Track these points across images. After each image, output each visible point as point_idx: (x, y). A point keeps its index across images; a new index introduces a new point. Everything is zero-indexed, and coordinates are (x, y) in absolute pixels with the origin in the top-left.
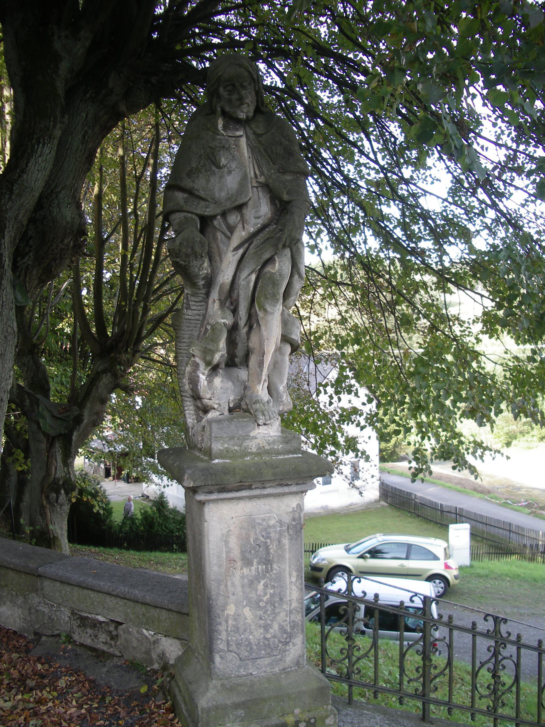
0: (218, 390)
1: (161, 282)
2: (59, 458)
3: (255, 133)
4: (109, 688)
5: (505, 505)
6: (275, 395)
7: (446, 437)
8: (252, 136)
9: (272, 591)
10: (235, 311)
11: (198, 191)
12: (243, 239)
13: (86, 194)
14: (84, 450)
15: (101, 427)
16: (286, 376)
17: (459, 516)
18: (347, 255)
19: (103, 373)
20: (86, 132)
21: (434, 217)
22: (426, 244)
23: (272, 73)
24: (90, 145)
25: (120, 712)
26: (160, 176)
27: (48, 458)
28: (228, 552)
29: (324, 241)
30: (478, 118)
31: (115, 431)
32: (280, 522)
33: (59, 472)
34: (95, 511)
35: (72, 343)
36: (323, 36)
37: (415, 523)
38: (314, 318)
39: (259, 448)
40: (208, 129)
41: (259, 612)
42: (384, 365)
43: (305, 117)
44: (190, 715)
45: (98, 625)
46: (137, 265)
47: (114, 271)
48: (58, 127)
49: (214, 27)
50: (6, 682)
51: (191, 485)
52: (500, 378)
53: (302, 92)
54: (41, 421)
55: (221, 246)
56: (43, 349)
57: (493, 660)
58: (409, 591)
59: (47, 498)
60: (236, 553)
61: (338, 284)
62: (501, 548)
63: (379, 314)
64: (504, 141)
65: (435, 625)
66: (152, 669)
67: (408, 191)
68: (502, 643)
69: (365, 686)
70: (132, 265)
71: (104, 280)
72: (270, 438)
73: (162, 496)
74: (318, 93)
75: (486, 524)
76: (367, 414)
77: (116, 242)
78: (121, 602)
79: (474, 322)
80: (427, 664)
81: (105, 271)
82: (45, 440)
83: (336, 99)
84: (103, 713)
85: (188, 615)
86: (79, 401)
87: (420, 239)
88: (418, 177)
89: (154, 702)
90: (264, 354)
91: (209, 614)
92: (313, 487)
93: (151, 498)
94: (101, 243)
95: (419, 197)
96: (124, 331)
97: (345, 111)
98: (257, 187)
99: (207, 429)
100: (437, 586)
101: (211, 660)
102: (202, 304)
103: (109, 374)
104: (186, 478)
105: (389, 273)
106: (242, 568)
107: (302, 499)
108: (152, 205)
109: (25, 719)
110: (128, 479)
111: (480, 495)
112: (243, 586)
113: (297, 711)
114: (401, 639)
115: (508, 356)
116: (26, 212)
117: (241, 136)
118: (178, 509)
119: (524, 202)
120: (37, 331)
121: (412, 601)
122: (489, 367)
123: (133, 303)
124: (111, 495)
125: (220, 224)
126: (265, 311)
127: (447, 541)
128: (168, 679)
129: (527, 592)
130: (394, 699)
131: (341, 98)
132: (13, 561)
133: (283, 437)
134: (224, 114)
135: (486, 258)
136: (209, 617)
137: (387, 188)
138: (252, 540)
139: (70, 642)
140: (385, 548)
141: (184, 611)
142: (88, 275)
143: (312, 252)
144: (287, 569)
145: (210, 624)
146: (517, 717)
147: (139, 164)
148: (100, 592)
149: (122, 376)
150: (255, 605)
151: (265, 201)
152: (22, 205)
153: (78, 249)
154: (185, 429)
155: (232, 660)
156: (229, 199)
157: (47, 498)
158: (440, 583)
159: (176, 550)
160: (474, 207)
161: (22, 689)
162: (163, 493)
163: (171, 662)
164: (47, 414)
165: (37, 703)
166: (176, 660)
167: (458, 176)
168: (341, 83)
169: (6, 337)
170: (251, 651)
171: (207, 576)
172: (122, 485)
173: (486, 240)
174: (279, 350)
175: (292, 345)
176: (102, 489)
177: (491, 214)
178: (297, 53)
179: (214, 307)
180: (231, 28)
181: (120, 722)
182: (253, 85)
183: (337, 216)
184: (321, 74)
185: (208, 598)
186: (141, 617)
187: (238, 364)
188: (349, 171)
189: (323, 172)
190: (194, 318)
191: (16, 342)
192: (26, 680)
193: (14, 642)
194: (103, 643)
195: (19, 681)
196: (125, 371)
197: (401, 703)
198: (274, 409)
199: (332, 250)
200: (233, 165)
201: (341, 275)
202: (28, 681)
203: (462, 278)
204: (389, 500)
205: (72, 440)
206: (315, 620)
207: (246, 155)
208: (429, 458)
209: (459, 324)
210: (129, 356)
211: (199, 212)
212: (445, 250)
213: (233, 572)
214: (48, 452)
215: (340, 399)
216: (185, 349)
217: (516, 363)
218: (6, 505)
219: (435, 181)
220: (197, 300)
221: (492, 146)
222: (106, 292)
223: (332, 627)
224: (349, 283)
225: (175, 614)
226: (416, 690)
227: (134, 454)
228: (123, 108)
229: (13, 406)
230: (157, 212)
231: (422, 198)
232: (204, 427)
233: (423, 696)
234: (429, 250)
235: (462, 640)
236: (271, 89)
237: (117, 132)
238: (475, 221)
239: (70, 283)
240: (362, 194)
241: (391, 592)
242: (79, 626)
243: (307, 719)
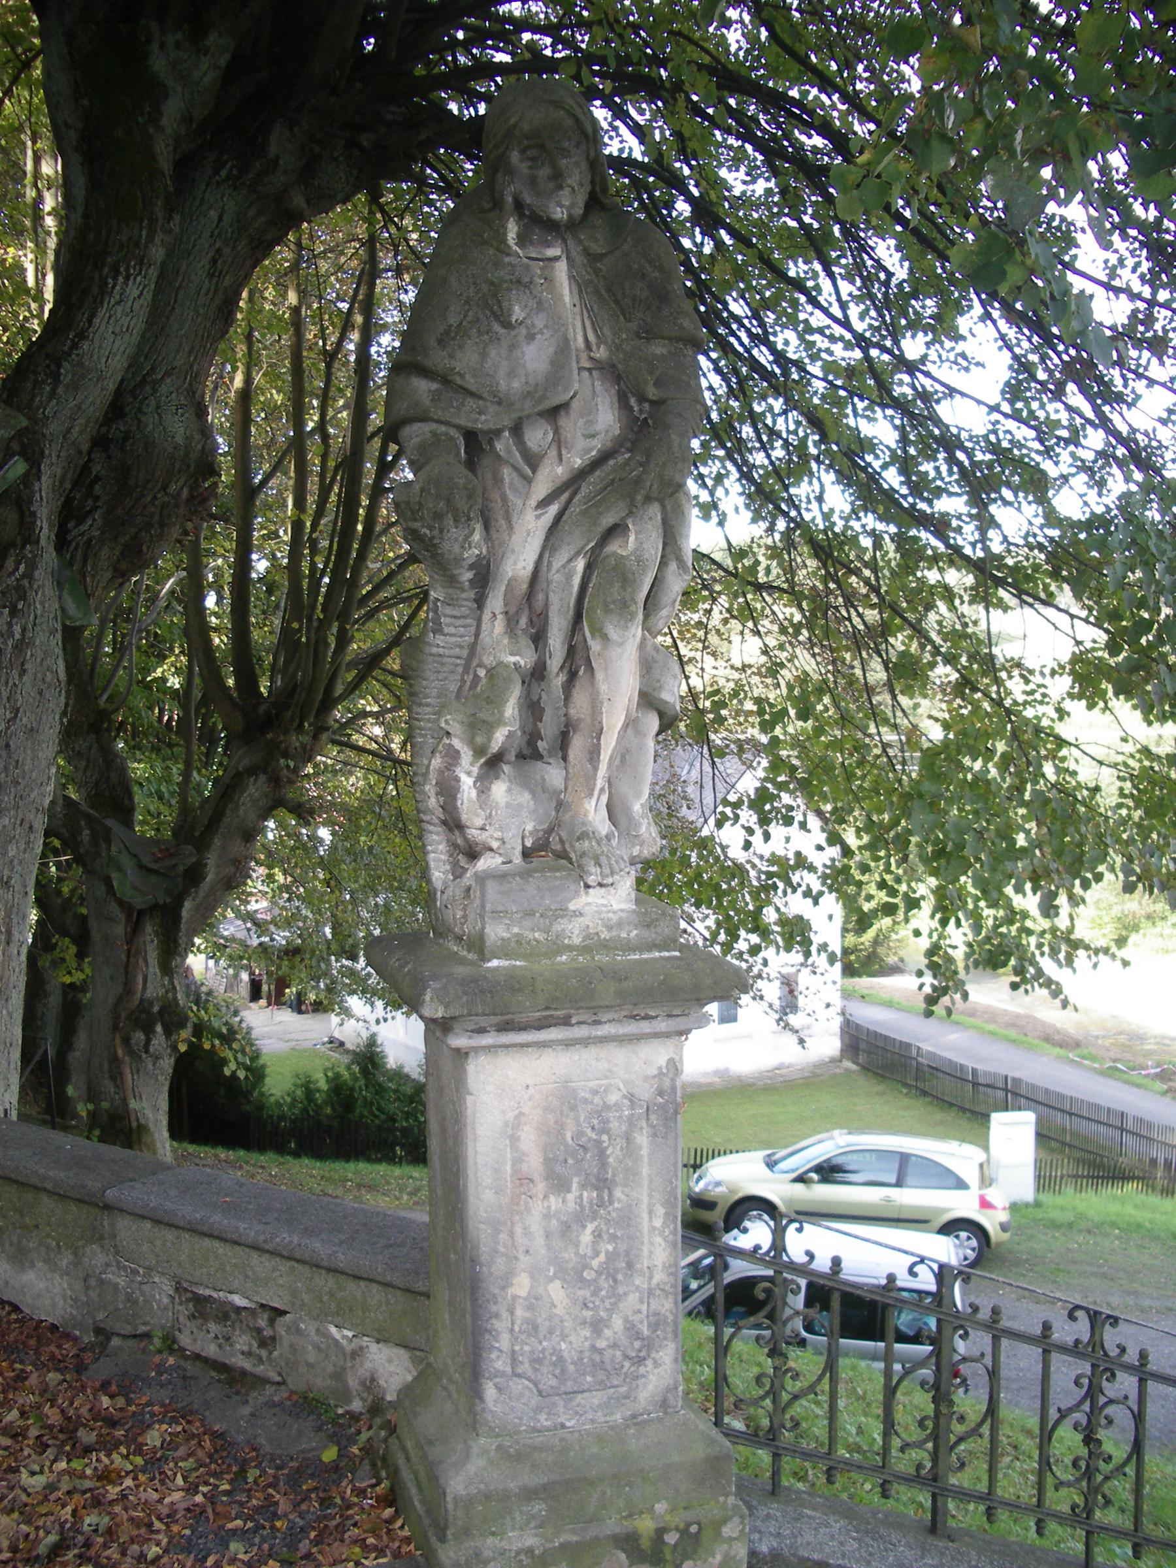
0: (500, 812)
1: (376, 580)
2: (153, 955)
3: (586, 252)
4: (254, 1449)
5: (1111, 1073)
6: (623, 822)
7: (996, 918)
8: (579, 259)
9: (610, 1248)
10: (539, 638)
11: (462, 376)
12: (558, 483)
13: (216, 388)
14: (207, 941)
15: (243, 892)
16: (649, 778)
17: (1013, 1095)
18: (781, 525)
19: (250, 775)
20: (218, 251)
21: (969, 445)
22: (953, 504)
23: (623, 130)
24: (228, 280)
25: (277, 1503)
26: (377, 352)
27: (128, 956)
28: (517, 1161)
29: (732, 496)
30: (1069, 231)
31: (274, 903)
32: (631, 1098)
33: (151, 984)
34: (227, 1072)
35: (185, 707)
36: (733, 49)
37: (917, 1108)
38: (709, 661)
39: (588, 937)
40: (485, 243)
41: (581, 1293)
42: (861, 763)
43: (693, 226)
44: (428, 1512)
45: (233, 1316)
46: (326, 544)
47: (274, 556)
48: (157, 240)
49: (498, 27)
50: (34, 1432)
51: (440, 1015)
52: (1108, 799)
53: (686, 171)
54: (115, 877)
55: (511, 496)
56: (122, 723)
57: (1086, 1407)
58: (906, 1252)
59: (126, 1041)
60: (534, 1164)
61: (759, 588)
62: (1101, 1166)
63: (848, 656)
64: (1125, 280)
65: (961, 1327)
66: (347, 1412)
67: (914, 388)
68: (1106, 1369)
69: (806, 1455)
70: (314, 544)
71: (254, 575)
72: (611, 915)
73: (372, 1042)
74: (723, 173)
75: (1071, 1114)
76: (825, 866)
77: (280, 493)
78: (284, 1266)
79: (1053, 673)
80: (944, 1410)
81: (254, 557)
82: (122, 917)
83: (760, 187)
84: (242, 1504)
85: (427, 1295)
86: (197, 834)
87: (938, 492)
88: (940, 357)
89: (351, 1481)
90: (601, 732)
91: (472, 1294)
92: (704, 1020)
93: (349, 1046)
94: (248, 493)
95: (938, 401)
96: (296, 686)
97: (780, 214)
98: (589, 370)
99: (476, 893)
100: (961, 1246)
101: (476, 1393)
102: (469, 621)
103: (262, 778)
104: (427, 998)
105: (873, 566)
106: (545, 1197)
107: (679, 1048)
108: (360, 414)
109: (74, 1512)
110: (298, 1006)
111: (1058, 1051)
112: (548, 1236)
113: (661, 1507)
114: (888, 1357)
115: (1129, 748)
116: (88, 422)
117: (556, 259)
118: (406, 1070)
119: (1165, 415)
120: (109, 682)
121: (912, 1272)
122: (1086, 773)
123: (315, 624)
124: (264, 1038)
125: (509, 452)
126: (605, 638)
127: (986, 1148)
128: (383, 1433)
129: (1157, 1262)
130: (868, 1486)
131: (772, 184)
132: (51, 1174)
133: (638, 914)
135: (1083, 536)
136: (474, 1300)
137: (873, 382)
138: (568, 1135)
139: (171, 1351)
140: (850, 1162)
141: (420, 1286)
142: (219, 564)
143: (706, 517)
144: (645, 1200)
145: (476, 1317)
146: (1136, 1530)
147: (332, 324)
148: (239, 1244)
149: (291, 782)
150: (574, 1276)
151: (608, 400)
152: (79, 409)
153: (199, 503)
154: (426, 897)
155: (521, 1395)
156: (528, 395)
157: (126, 1041)
158: (969, 1238)
159: (401, 1158)
160: (1057, 424)
161: (68, 1448)
162: (373, 1035)
163: (389, 1398)
164: (126, 861)
165: (100, 1478)
166: (399, 1392)
167: (1025, 356)
168: (772, 152)
169: (40, 693)
170: (563, 1376)
171: (471, 1212)
172: (286, 1017)
173: (1081, 496)
174: (631, 724)
175: (661, 715)
176: (244, 1025)
177: (1095, 439)
178: (677, 87)
179: (495, 629)
180: (535, 29)
181: (278, 1524)
182: (583, 147)
183: (760, 440)
184: (728, 131)
185: (472, 1261)
186: (325, 1298)
187: (544, 753)
188: (787, 343)
189: (732, 345)
190: (452, 652)
191: (62, 705)
192: (76, 1430)
193: (53, 1348)
194: (243, 1353)
195: (61, 1431)
196: (296, 771)
197: (885, 1495)
198: (622, 851)
199: (749, 515)
200: (539, 321)
201: (769, 571)
202: (81, 1433)
203: (1028, 578)
204: (861, 1058)
205: (179, 917)
206: (698, 1314)
207: (567, 299)
208: (961, 965)
209: (1022, 676)
210: (305, 739)
211: (463, 422)
212: (992, 516)
213: (526, 1204)
214: (129, 942)
215: (767, 837)
216: (429, 720)
217: (1147, 763)
218: (37, 1058)
219: (972, 367)
220: (458, 614)
221: (1099, 292)
222: (258, 599)
223: (739, 1328)
224: (785, 586)
225: (399, 1293)
226: (919, 1467)
227: (313, 952)
228: (298, 201)
229: (57, 843)
230: (370, 429)
231: (943, 402)
232: (468, 889)
233: (932, 1480)
234: (959, 518)
235: (1021, 1361)
236: (622, 164)
237: (283, 255)
238: (1057, 455)
239: (182, 580)
240: (816, 393)
241: (868, 1257)
242: (192, 1317)
243: (682, 1526)
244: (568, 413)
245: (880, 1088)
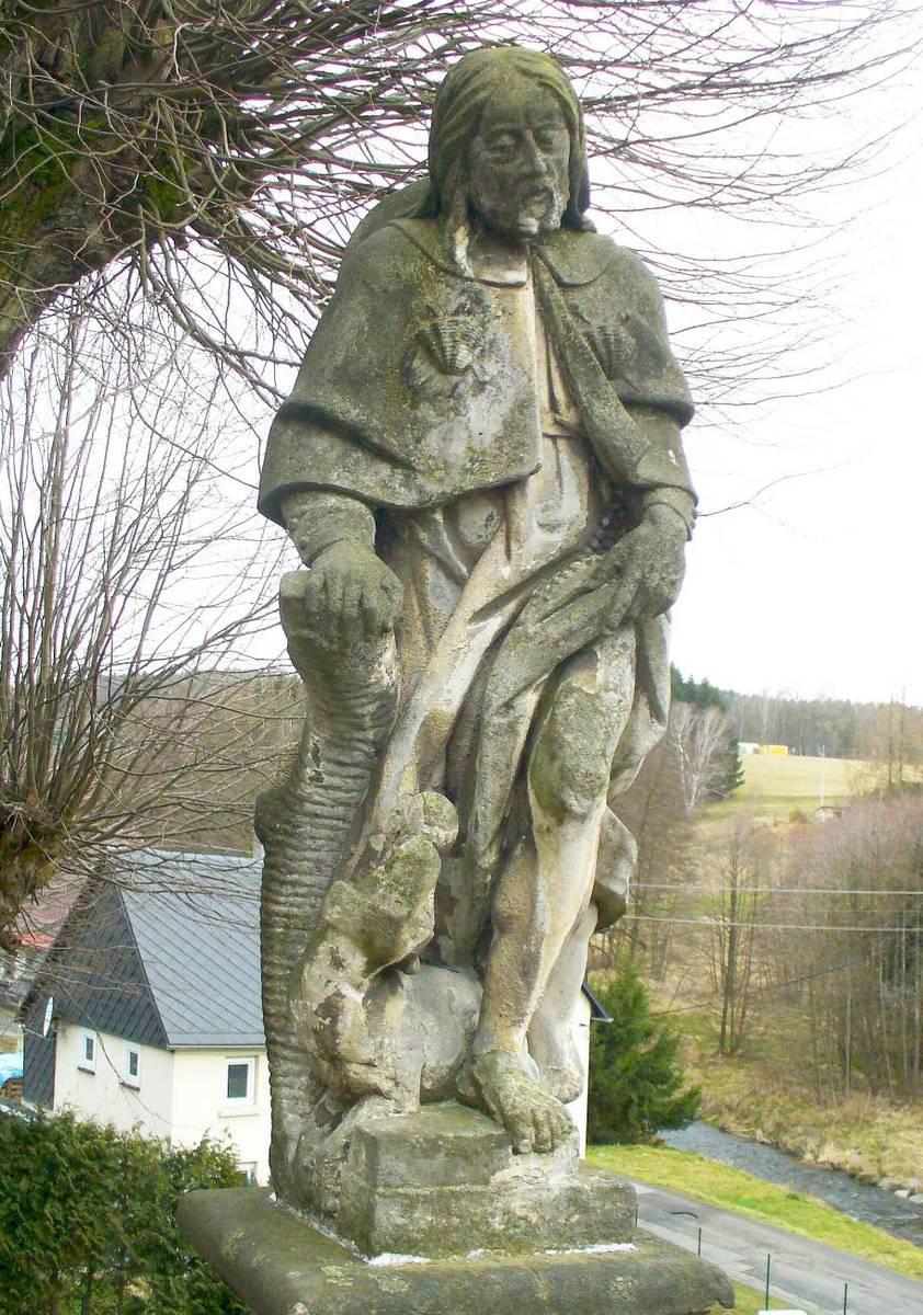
98: (554, 438)
117: (519, 285)
134: (474, 216)
244: (524, 495)
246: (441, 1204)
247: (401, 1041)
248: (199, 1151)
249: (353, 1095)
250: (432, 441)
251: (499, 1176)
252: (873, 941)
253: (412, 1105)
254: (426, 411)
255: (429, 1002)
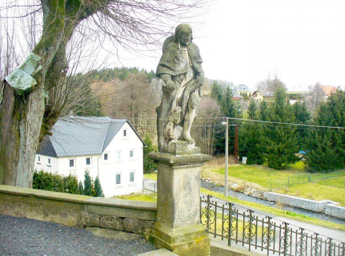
60: (182, 186)
112: (183, 197)
117: (186, 50)
150: (186, 203)
211: (171, 74)
245: (300, 212)
246: (182, 150)
247: (175, 133)
248: (69, 176)
249: (170, 140)
250: (177, 68)
251: (187, 147)
252: (199, 129)
253: (177, 140)
254: (176, 65)
255: (178, 129)
